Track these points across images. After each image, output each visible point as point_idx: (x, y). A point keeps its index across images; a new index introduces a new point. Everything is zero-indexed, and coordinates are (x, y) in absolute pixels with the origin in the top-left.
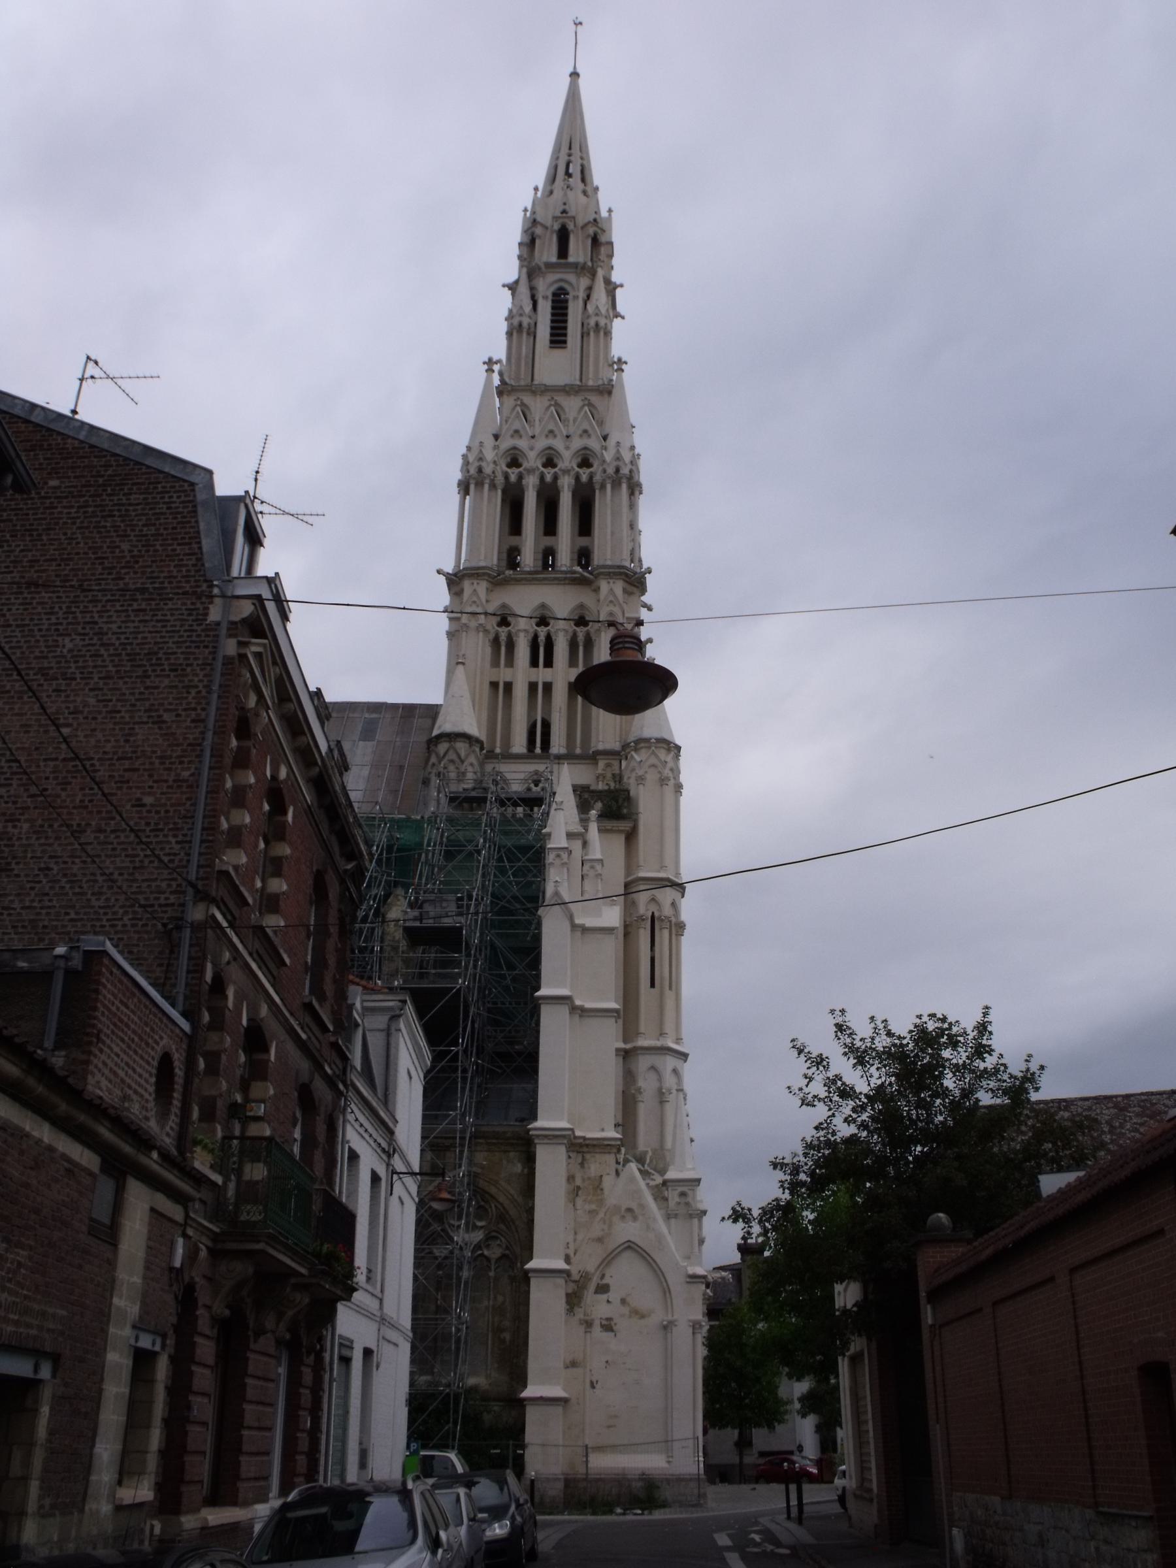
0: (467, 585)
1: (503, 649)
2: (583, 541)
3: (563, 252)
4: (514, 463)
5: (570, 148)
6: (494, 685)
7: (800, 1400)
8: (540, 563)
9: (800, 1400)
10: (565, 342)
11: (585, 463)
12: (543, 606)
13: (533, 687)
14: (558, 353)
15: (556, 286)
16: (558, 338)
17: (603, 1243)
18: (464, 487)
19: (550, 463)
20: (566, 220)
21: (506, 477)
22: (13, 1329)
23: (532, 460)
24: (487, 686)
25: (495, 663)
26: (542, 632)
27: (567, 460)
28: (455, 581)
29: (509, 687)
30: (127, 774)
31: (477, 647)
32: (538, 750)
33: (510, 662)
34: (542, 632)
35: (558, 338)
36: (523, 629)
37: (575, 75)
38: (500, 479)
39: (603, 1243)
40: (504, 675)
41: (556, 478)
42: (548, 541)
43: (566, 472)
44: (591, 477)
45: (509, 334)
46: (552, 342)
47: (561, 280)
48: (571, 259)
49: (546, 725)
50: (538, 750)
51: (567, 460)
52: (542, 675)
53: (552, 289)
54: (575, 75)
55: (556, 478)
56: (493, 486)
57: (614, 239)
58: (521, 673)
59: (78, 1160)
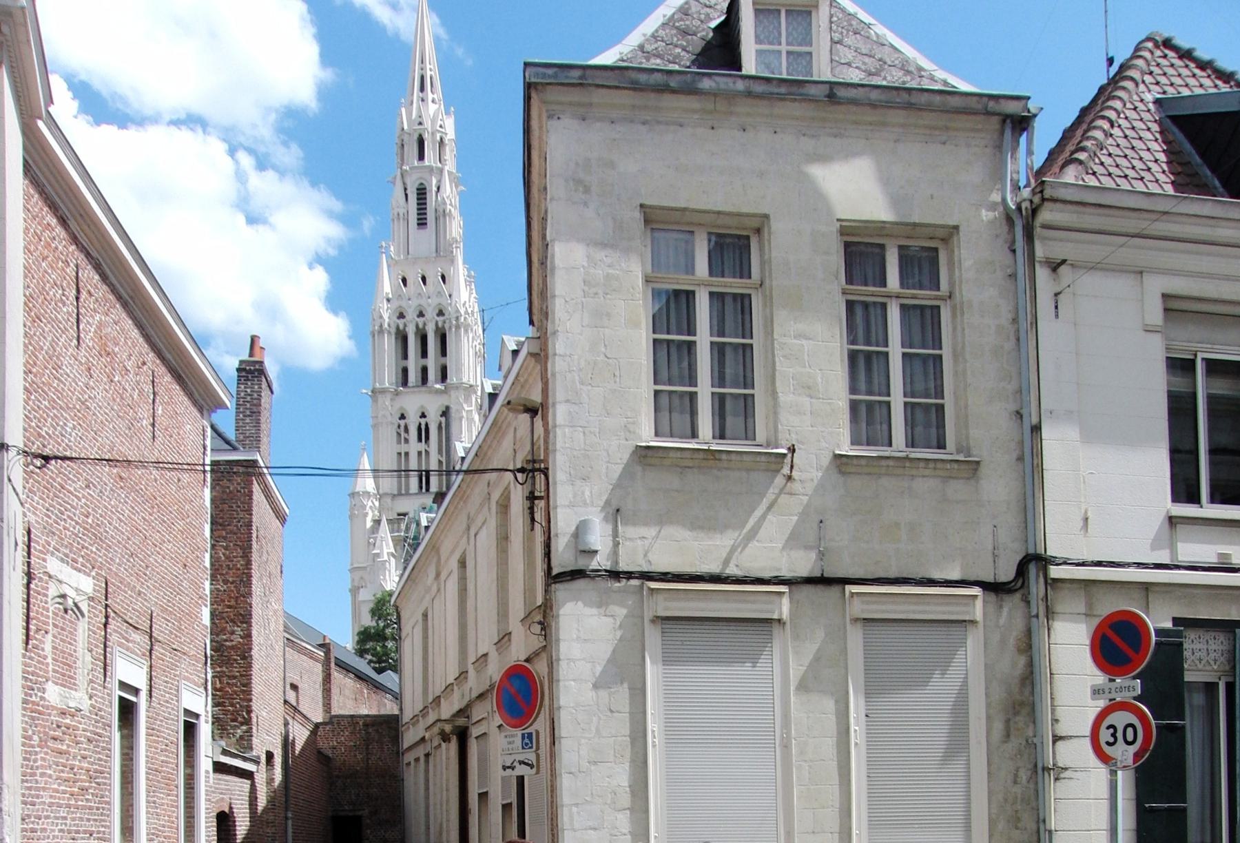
1: (402, 433)
2: (442, 360)
3: (421, 157)
4: (401, 316)
5: (422, 63)
6: (400, 454)
7: (434, 502)
8: (420, 379)
9: (434, 502)
10: (426, 224)
11: (441, 313)
12: (422, 407)
13: (420, 453)
14: (422, 232)
15: (418, 182)
16: (422, 223)
17: (349, 495)
19: (421, 314)
20: (422, 132)
23: (411, 315)
24: (396, 454)
25: (399, 442)
26: (423, 421)
27: (431, 314)
29: (407, 454)
30: (88, 339)
32: (424, 490)
34: (423, 421)
35: (422, 223)
36: (413, 422)
38: (393, 330)
39: (349, 495)
40: (403, 448)
42: (423, 362)
46: (418, 224)
47: (421, 178)
48: (427, 163)
50: (424, 490)
51: (431, 314)
53: (416, 185)
56: (389, 333)
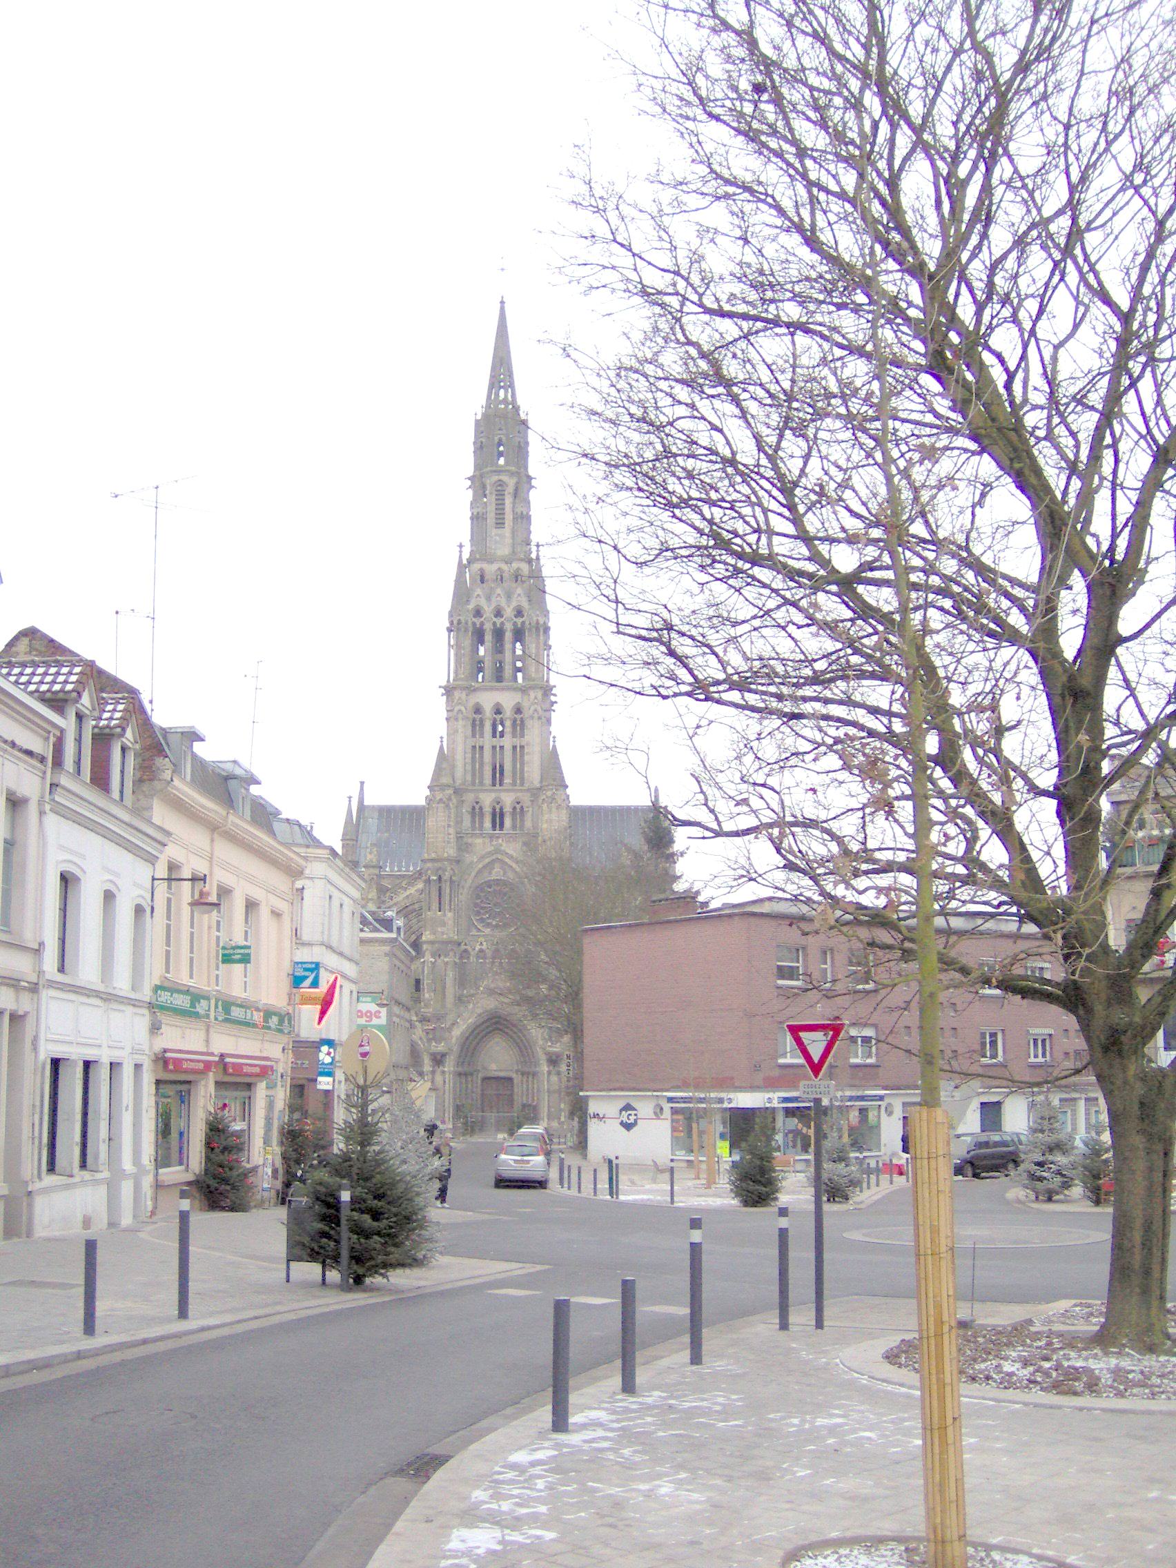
0: (457, 694)
1: (476, 726)
13: (494, 747)
18: (450, 630)
21: (474, 624)
22: (1104, 814)
25: (474, 736)
27: (509, 612)
28: (449, 691)
29: (482, 748)
31: (463, 727)
33: (482, 736)
37: (502, 302)
40: (479, 742)
41: (502, 623)
42: (499, 656)
43: (509, 620)
44: (523, 623)
45: (472, 519)
49: (502, 767)
52: (497, 742)
54: (502, 302)
55: (502, 623)
57: (533, 513)
58: (487, 741)
59: (243, 995)
